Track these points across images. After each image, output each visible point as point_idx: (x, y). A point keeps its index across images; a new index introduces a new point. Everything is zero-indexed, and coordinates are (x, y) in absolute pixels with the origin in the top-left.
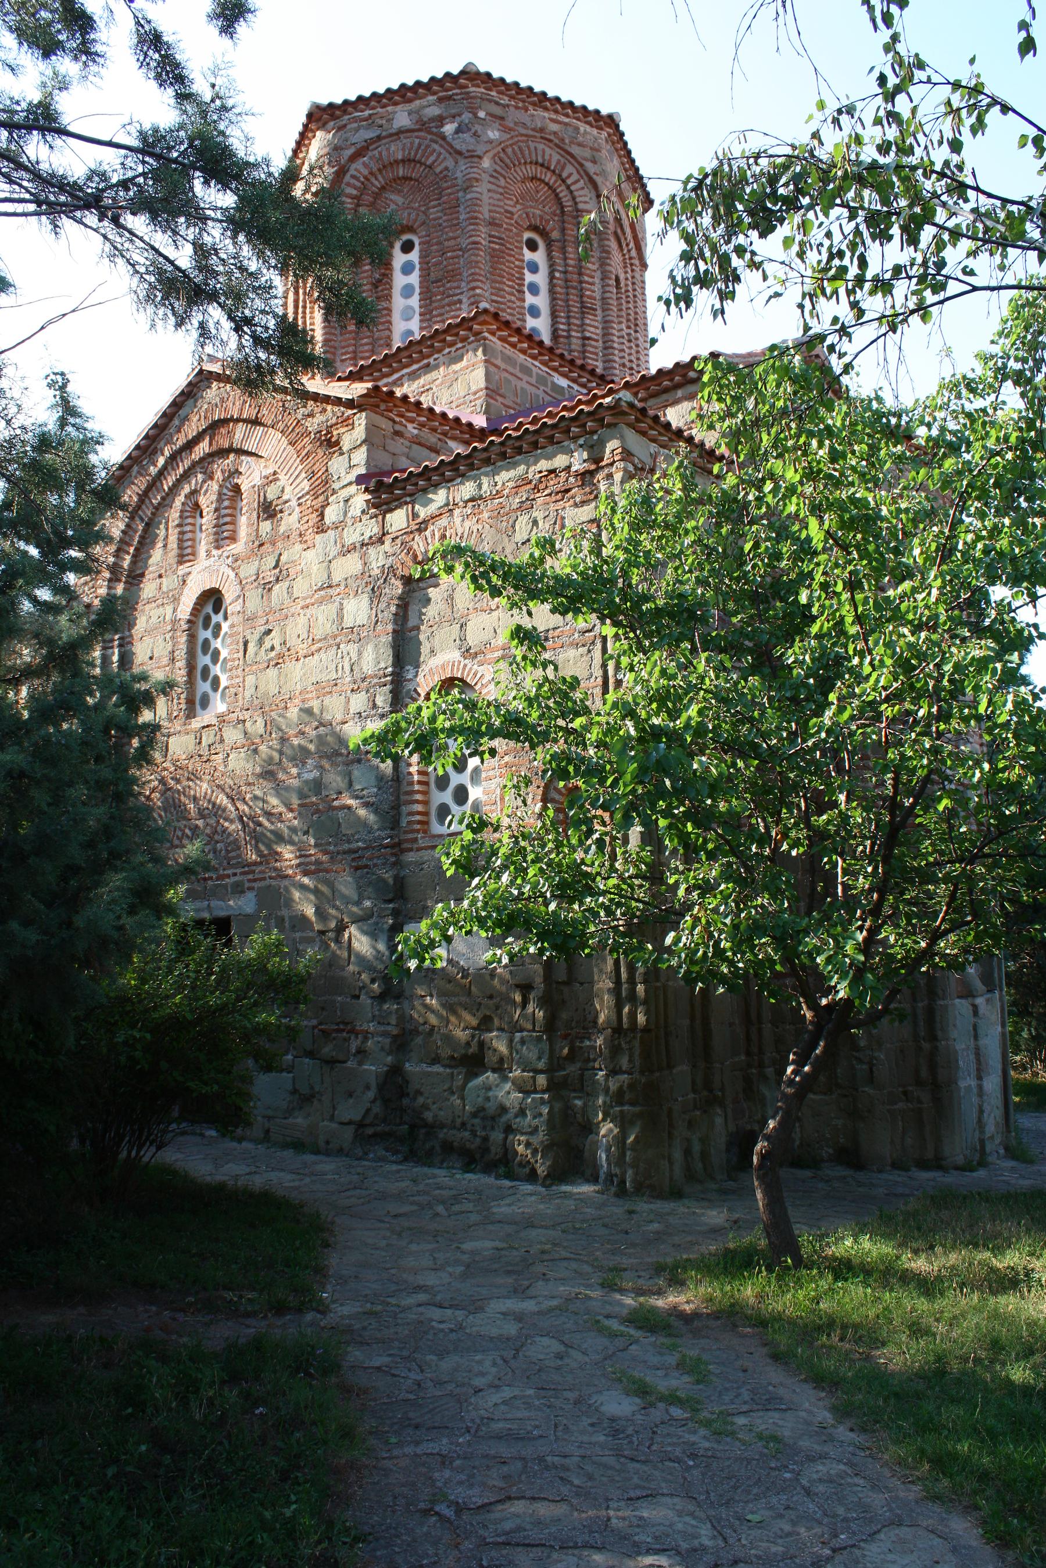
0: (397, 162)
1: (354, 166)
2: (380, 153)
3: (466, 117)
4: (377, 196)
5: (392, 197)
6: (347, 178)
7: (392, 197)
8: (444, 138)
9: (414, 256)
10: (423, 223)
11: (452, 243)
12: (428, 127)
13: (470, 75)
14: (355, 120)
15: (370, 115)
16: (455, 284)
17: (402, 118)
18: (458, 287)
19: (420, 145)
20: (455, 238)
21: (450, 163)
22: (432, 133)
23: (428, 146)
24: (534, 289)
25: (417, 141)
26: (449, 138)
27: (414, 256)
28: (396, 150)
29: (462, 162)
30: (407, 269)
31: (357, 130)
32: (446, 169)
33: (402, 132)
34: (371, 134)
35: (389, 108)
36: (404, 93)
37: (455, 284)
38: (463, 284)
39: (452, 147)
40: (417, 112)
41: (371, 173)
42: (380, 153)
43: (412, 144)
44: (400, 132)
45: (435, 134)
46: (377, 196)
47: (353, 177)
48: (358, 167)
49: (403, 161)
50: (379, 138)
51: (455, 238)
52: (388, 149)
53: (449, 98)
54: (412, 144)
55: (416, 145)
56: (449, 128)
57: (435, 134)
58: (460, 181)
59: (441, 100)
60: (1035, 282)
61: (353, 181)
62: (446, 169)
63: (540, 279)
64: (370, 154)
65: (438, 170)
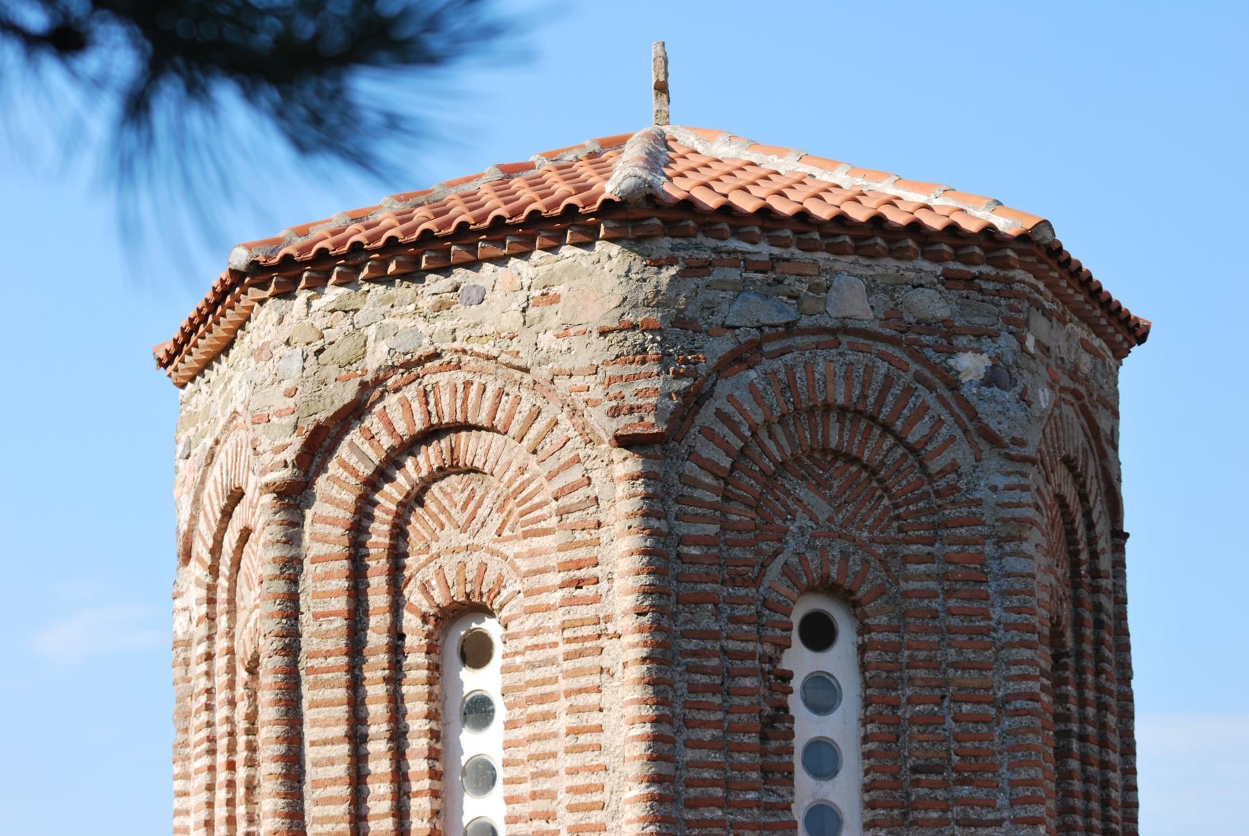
0: (827, 407)
1: (724, 387)
2: (790, 370)
3: (1006, 342)
4: (769, 479)
5: (801, 492)
6: (706, 416)
7: (801, 492)
8: (954, 385)
9: (839, 661)
10: (881, 592)
11: (971, 678)
12: (927, 343)
13: (1039, 247)
14: (737, 260)
15: (774, 259)
16: (981, 794)
17: (851, 295)
18: (989, 804)
19: (888, 381)
20: (981, 668)
21: (961, 453)
22: (925, 362)
23: (908, 391)
24: (823, 759)
25: (883, 367)
26: (970, 392)
27: (839, 661)
28: (831, 375)
29: (993, 462)
30: (823, 694)
31: (741, 289)
32: (954, 468)
33: (846, 331)
34: (771, 313)
35: (821, 256)
36: (876, 236)
37: (981, 794)
38: (1002, 800)
39: (974, 415)
40: (892, 288)
41: (768, 425)
42: (790, 370)
43: (869, 369)
44: (844, 330)
45: (933, 368)
46: (769, 479)
47: (721, 416)
48: (735, 390)
49: (843, 410)
50: (790, 328)
51: (981, 668)
52: (809, 367)
53: (969, 281)
54: (869, 369)
55: (878, 377)
56: (970, 364)
57: (933, 368)
58: (987, 514)
59: (949, 279)
60: (528, 198)
61: (721, 429)
62: (954, 468)
63: (841, 726)
64: (767, 365)
65: (935, 466)
